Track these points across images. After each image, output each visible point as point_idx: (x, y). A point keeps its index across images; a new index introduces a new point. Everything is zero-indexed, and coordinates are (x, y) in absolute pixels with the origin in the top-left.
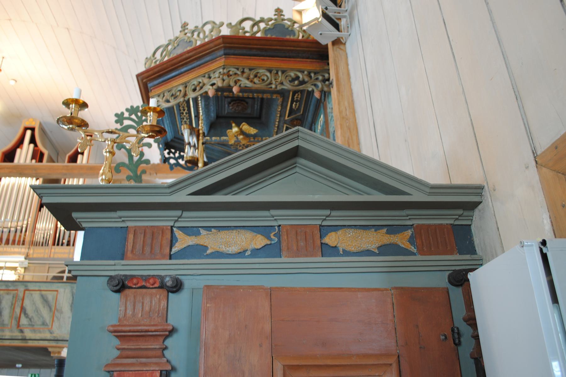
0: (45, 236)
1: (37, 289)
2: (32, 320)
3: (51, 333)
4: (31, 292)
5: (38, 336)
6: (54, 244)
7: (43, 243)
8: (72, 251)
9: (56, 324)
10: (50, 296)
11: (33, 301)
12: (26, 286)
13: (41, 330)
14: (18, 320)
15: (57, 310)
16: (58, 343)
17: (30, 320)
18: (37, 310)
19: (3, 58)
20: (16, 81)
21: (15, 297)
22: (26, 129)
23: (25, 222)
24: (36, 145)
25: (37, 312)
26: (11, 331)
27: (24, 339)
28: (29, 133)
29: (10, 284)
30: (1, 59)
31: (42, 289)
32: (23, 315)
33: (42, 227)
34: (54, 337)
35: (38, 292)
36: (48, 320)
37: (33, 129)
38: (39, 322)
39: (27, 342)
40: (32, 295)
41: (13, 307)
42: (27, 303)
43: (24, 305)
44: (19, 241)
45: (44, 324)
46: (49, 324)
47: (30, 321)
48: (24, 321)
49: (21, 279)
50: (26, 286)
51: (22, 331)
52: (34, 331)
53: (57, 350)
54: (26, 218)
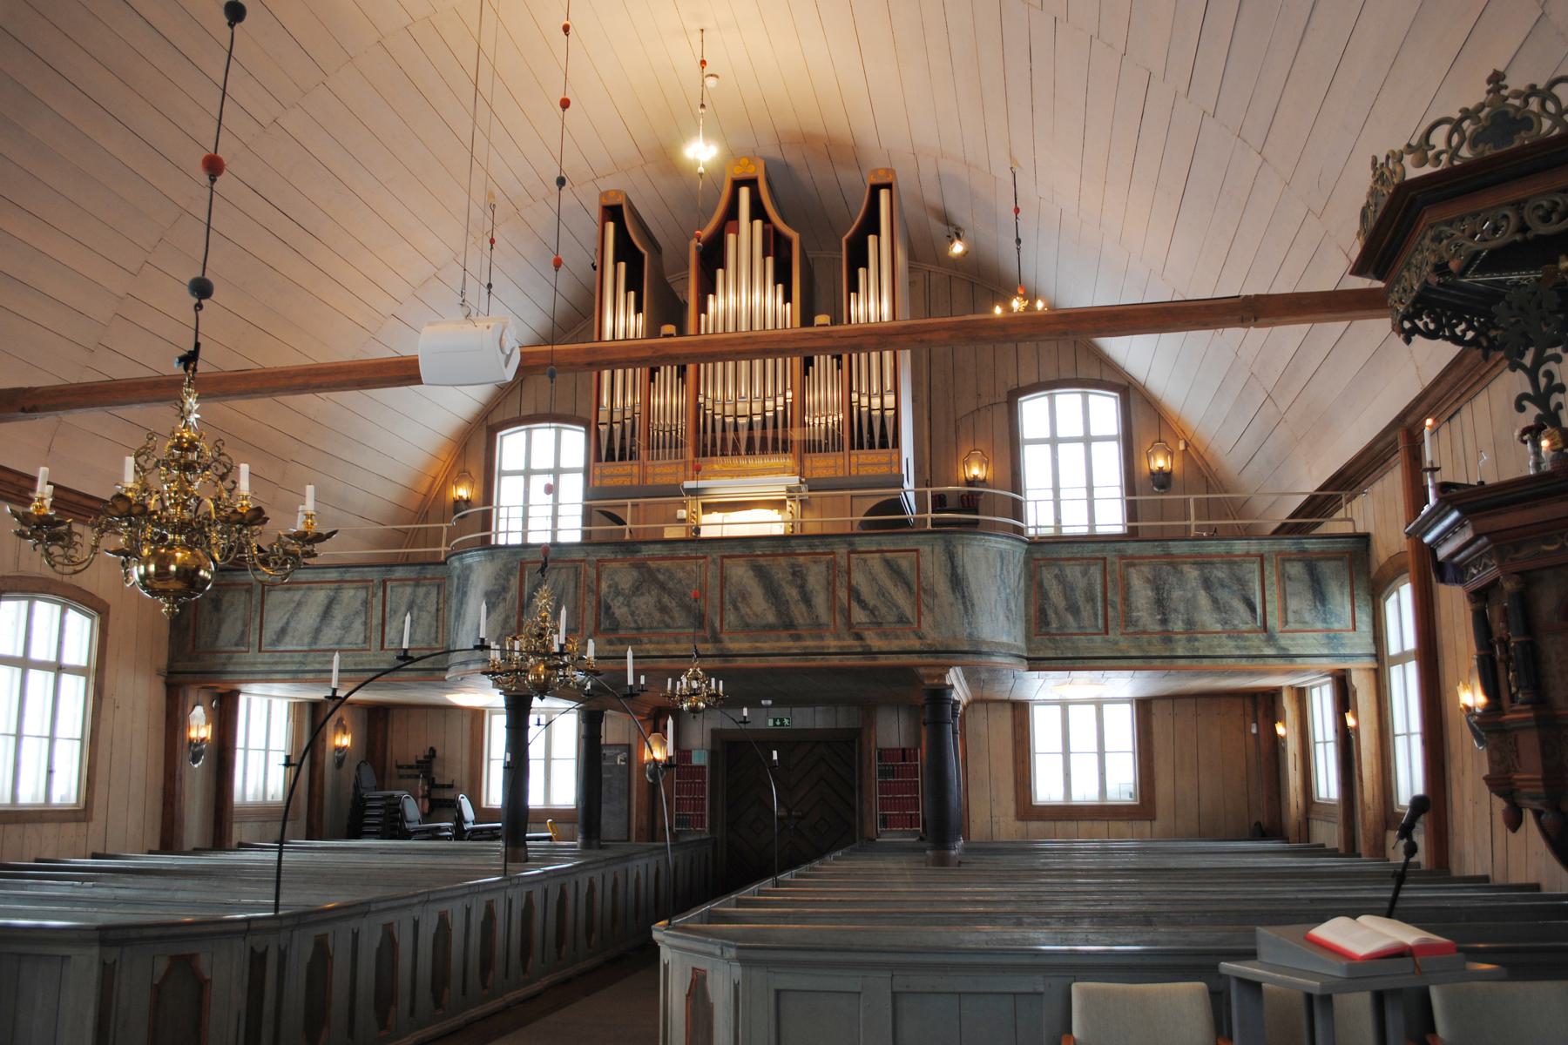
0: (830, 425)
1: (874, 549)
2: (876, 613)
3: (920, 638)
4: (863, 556)
5: (895, 645)
6: (852, 448)
7: (827, 444)
8: (895, 457)
9: (926, 621)
10: (905, 563)
11: (870, 573)
12: (851, 544)
13: (899, 632)
14: (846, 614)
15: (925, 591)
16: (938, 658)
17: (872, 612)
18: (882, 593)
19: (702, 30)
20: (717, 77)
21: (832, 566)
22: (737, 184)
23: (780, 400)
24: (766, 220)
25: (883, 596)
26: (838, 637)
27: (868, 653)
28: (744, 193)
29: (817, 542)
30: (700, 34)
31: (885, 548)
32: (854, 604)
33: (882, 409)
34: (929, 645)
35: (877, 555)
36: (909, 613)
37: (751, 183)
38: (892, 618)
39: (875, 659)
40: (865, 561)
41: (830, 588)
42: (859, 579)
43: (854, 582)
44: (611, 450)
45: (902, 619)
46: (911, 620)
47: (872, 616)
48: (859, 615)
49: (798, 532)
50: (851, 544)
51: (859, 637)
52: (884, 635)
53: (939, 671)
54: (780, 391)
